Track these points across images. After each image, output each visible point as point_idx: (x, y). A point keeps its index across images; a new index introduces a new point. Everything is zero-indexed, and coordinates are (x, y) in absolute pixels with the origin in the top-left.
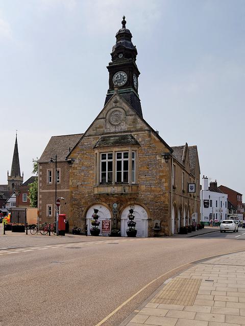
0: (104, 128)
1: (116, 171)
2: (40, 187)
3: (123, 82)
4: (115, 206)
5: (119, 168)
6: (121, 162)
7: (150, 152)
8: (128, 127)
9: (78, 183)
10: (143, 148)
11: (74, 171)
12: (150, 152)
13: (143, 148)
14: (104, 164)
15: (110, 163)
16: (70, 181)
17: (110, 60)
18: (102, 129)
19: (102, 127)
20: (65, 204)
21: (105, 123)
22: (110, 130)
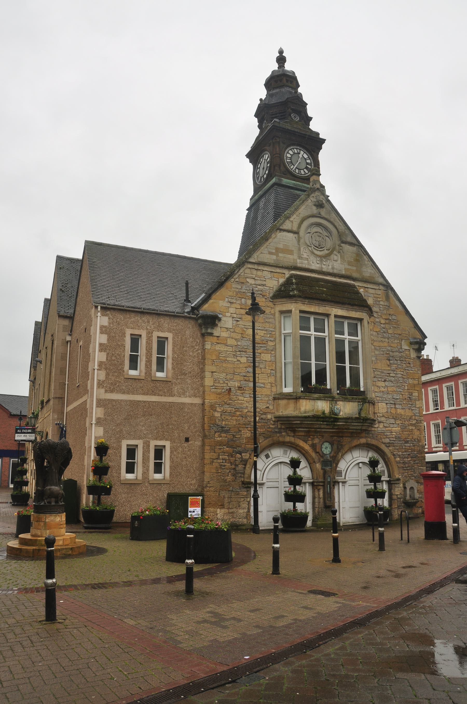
0: (295, 256)
1: (361, 366)
2: (100, 384)
3: (289, 156)
4: (327, 449)
5: (340, 357)
6: (309, 338)
7: (390, 331)
8: (348, 267)
9: (231, 384)
10: (377, 320)
11: (218, 347)
12: (390, 331)
13: (377, 320)
14: (305, 340)
15: (320, 342)
16: (208, 374)
17: (263, 93)
18: (291, 257)
19: (291, 252)
20: (187, 440)
21: (296, 244)
22: (309, 264)
